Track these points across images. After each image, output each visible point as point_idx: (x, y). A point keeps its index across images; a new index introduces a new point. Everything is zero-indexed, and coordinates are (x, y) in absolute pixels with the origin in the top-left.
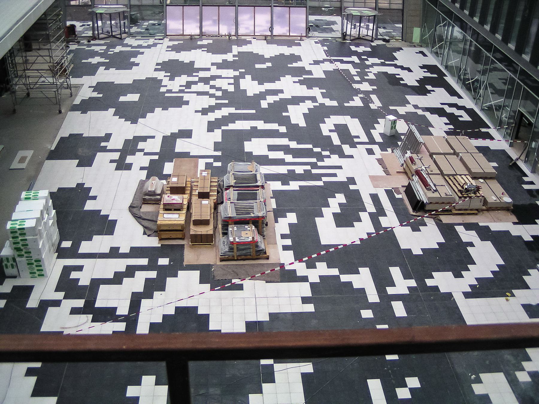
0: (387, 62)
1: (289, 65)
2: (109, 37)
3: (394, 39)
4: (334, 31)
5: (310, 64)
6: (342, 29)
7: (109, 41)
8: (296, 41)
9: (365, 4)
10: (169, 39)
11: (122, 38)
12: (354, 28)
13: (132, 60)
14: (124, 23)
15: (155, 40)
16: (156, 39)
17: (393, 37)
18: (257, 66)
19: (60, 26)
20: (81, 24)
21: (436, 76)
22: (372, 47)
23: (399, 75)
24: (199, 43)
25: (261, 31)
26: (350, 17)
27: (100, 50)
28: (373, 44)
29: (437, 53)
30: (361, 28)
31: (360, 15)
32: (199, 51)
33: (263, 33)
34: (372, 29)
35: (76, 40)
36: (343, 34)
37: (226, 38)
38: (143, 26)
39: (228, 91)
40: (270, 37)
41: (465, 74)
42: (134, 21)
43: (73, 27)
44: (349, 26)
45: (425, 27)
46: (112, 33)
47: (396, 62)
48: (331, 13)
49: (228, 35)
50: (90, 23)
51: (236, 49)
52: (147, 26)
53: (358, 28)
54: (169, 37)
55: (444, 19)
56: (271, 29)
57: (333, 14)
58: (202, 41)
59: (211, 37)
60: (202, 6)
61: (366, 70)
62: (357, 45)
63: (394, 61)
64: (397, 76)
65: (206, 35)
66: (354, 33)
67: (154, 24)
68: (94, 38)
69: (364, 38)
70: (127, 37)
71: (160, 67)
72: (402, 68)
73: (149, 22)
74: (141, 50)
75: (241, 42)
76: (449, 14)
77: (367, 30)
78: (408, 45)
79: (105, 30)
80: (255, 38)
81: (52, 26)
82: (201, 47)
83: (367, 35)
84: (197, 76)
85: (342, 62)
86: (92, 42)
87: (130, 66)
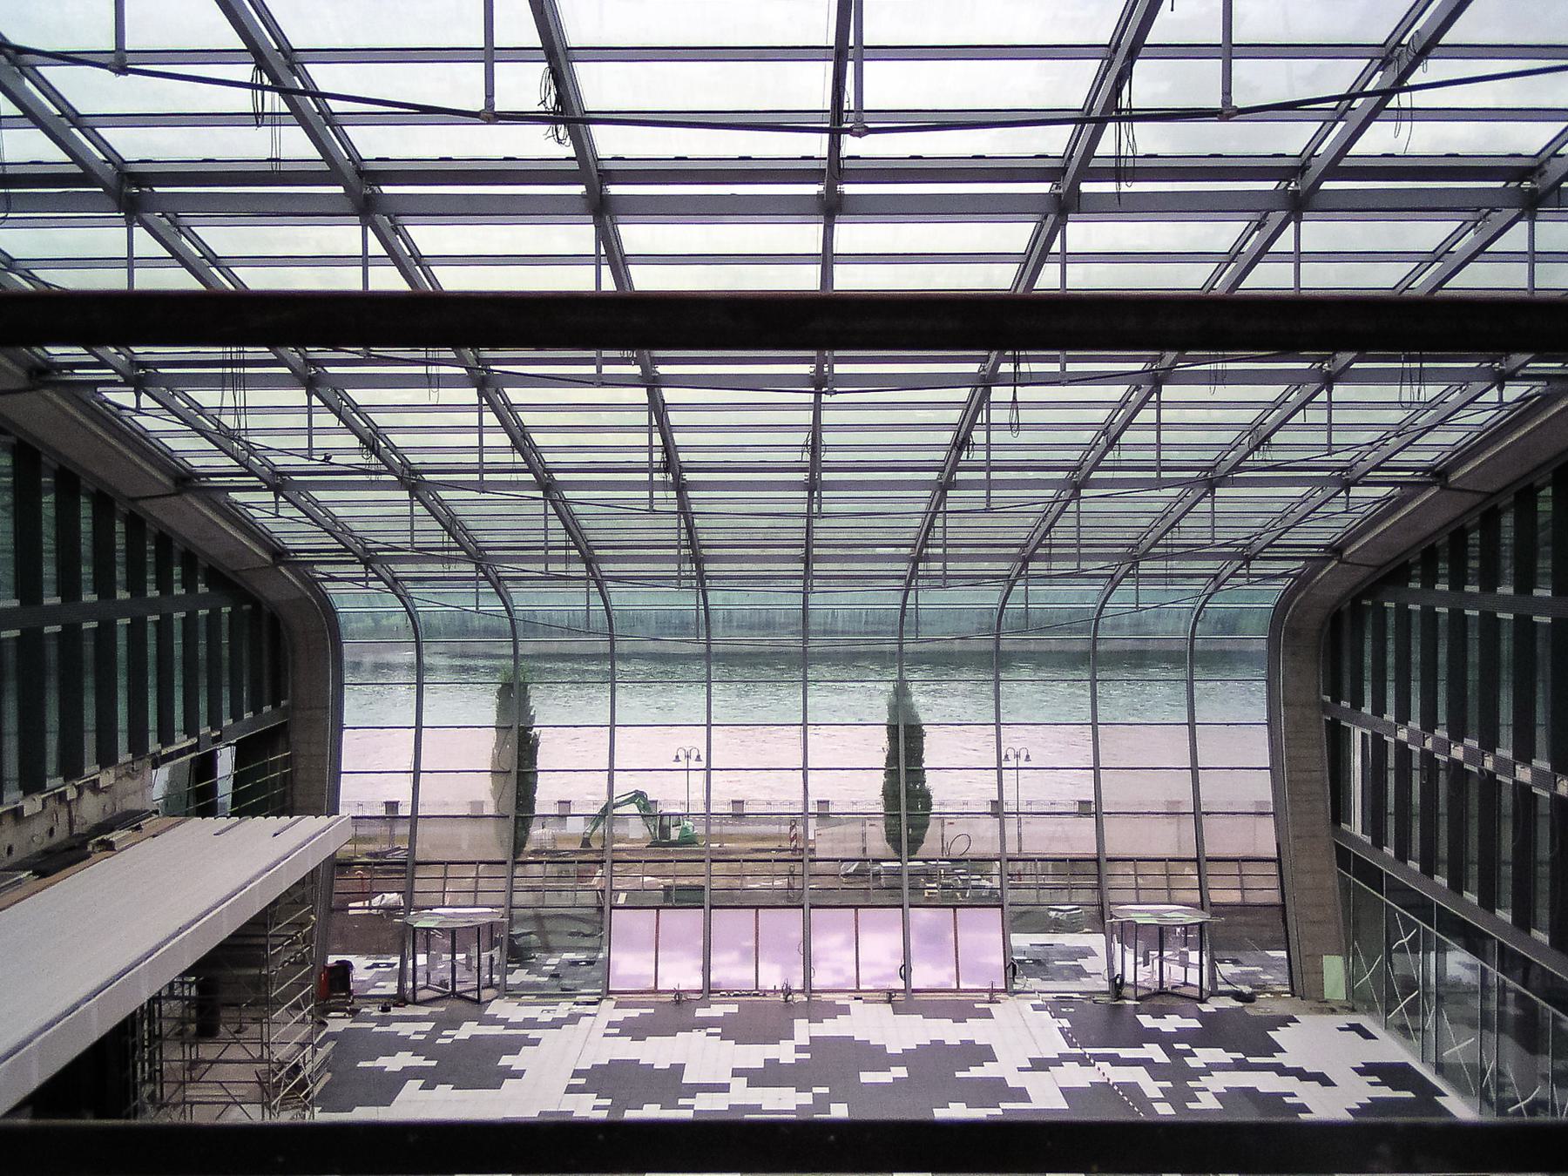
0: (1251, 1060)
1: (959, 1074)
2: (445, 997)
3: (1268, 992)
4: (1088, 975)
5: (1020, 1069)
6: (1111, 968)
7: (443, 1009)
8: (977, 1006)
9: (1169, 894)
10: (614, 1003)
11: (483, 999)
12: (1146, 963)
13: (505, 1060)
14: (492, 959)
15: (575, 1006)
16: (576, 1003)
17: (1263, 988)
18: (867, 1077)
19: (304, 955)
20: (370, 962)
21: (1409, 1094)
22: (1202, 1016)
23: (1292, 1095)
24: (701, 1013)
25: (874, 979)
26: (1128, 933)
27: (414, 1034)
28: (1205, 1008)
29: (1403, 1029)
30: (1164, 963)
31: (1156, 922)
32: (698, 1036)
33: (883, 983)
34: (1198, 962)
35: (349, 1004)
36: (1112, 981)
37: (775, 999)
38: (544, 968)
39: (763, 1108)
40: (902, 994)
41: (1500, 1088)
42: (518, 955)
43: (345, 967)
44: (1129, 957)
45: (1355, 950)
46: (454, 987)
47: (1278, 1058)
48: (1072, 927)
49: (782, 991)
50: (396, 960)
51: (804, 1030)
52: (554, 968)
53: (1157, 962)
54: (615, 997)
55: (1409, 925)
56: (906, 972)
57: (1081, 928)
58: (710, 1007)
59: (736, 995)
60: (712, 907)
61: (1191, 1084)
62: (1159, 1014)
63: (1274, 1056)
64: (1288, 1100)
65: (719, 992)
66: (1146, 976)
67: (575, 963)
68: (401, 999)
69: (1176, 991)
70: (496, 998)
71: (582, 1081)
72: (1301, 1074)
73: (558, 960)
74: (533, 1034)
75: (818, 1009)
76: (1422, 907)
77: (1183, 969)
78: (1311, 1009)
79: (435, 978)
80: (861, 999)
81: (281, 955)
82: (704, 1024)
83: (1186, 984)
84: (690, 1107)
85: (1116, 1061)
86: (395, 1012)
87: (495, 1078)
